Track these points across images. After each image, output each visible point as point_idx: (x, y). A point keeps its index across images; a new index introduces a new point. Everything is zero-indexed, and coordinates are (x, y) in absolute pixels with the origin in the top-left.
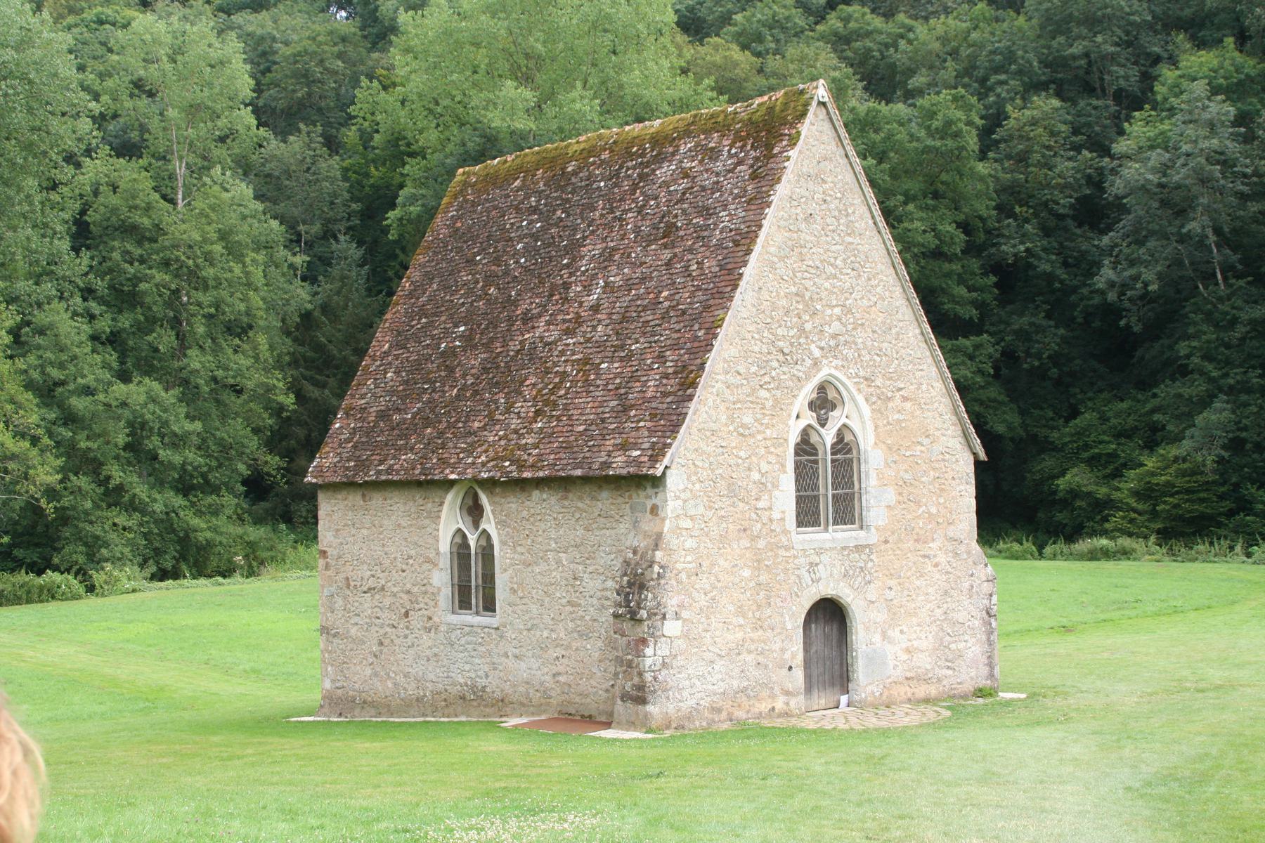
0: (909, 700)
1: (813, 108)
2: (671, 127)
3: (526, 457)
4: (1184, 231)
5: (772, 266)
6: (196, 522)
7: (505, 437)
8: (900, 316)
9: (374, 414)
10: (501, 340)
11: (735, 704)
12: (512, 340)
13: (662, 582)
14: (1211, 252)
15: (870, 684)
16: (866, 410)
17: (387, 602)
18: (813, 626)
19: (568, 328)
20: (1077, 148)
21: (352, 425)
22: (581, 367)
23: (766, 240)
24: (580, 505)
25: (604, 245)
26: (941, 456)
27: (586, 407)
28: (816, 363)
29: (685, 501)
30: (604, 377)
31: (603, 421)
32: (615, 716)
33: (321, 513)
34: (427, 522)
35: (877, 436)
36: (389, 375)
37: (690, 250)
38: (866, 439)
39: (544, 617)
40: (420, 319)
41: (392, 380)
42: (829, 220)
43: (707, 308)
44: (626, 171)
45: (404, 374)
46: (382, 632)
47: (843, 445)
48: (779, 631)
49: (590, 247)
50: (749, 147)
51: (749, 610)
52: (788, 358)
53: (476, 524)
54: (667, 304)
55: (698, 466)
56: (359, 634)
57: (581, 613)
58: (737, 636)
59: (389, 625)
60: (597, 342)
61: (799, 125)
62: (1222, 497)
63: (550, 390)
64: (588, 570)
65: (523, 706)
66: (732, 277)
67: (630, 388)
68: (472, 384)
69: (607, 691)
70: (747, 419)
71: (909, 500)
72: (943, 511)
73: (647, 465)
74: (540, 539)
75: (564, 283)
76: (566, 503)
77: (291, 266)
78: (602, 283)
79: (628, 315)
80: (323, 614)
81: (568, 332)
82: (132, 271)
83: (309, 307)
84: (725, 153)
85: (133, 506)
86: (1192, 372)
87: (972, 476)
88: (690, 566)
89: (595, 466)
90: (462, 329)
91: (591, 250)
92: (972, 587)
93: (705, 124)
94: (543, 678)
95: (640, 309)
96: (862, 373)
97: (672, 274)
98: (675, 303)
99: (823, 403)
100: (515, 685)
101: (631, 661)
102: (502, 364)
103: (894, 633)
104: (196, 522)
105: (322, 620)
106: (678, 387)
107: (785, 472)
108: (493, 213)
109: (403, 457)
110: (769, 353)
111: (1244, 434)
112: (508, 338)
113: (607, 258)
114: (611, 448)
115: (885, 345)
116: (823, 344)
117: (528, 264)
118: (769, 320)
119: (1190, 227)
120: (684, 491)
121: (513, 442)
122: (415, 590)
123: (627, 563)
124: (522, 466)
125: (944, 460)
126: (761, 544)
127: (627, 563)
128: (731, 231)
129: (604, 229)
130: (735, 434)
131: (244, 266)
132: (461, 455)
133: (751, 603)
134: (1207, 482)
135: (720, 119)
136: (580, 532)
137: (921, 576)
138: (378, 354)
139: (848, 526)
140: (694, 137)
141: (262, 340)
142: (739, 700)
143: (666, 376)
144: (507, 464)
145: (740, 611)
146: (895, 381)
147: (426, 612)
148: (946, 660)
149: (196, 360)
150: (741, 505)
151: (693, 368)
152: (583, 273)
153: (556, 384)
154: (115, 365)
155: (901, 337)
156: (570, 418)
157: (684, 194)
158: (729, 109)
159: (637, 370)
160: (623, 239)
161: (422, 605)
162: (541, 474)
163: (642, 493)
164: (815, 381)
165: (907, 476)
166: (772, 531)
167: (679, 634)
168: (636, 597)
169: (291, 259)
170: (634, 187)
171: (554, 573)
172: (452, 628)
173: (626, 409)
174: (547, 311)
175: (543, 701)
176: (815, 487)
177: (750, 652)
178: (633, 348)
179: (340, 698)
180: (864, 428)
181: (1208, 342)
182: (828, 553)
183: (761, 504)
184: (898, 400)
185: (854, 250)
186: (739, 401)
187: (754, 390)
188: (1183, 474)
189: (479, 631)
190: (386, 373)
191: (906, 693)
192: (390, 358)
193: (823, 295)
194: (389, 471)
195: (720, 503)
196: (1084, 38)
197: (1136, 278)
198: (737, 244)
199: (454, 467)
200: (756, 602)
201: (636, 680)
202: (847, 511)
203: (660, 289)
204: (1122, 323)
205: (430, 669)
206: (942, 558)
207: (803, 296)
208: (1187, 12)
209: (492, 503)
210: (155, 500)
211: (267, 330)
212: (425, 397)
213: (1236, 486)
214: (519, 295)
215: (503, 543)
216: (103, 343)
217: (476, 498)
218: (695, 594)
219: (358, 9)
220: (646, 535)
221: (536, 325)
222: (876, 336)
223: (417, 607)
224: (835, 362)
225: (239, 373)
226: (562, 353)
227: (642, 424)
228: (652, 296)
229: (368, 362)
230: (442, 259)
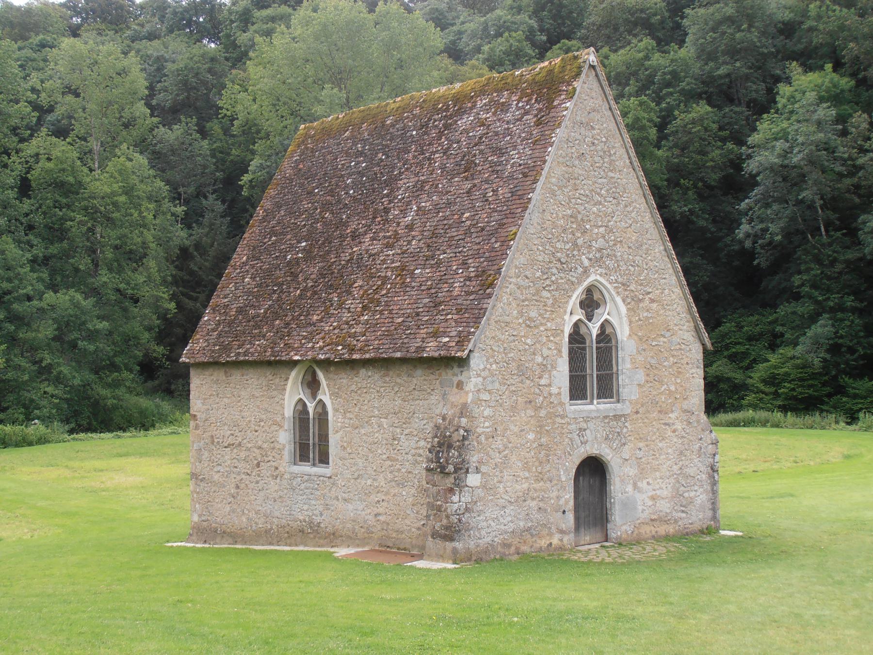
0: (653, 537)
1: (585, 70)
2: (469, 88)
3: (355, 343)
4: (800, 197)
6: (104, 392)
7: (339, 327)
8: (648, 236)
9: (235, 310)
10: (335, 252)
11: (522, 541)
12: (343, 252)
13: (466, 443)
14: (817, 212)
15: (625, 524)
16: (623, 309)
17: (243, 455)
18: (581, 478)
19: (388, 242)
20: (724, 140)
21: (217, 318)
22: (399, 272)
23: (549, 172)
24: (398, 380)
25: (417, 178)
26: (678, 346)
27: (403, 302)
28: (586, 272)
29: (484, 379)
30: (418, 280)
31: (418, 314)
32: (427, 549)
33: (192, 386)
34: (275, 393)
35: (631, 329)
36: (246, 280)
37: (487, 181)
38: (623, 331)
39: (369, 468)
40: (271, 237)
41: (249, 284)
42: (597, 159)
43: (501, 225)
44: (434, 123)
45: (258, 279)
46: (239, 478)
47: (606, 337)
48: (556, 482)
49: (405, 181)
50: (533, 101)
51: (533, 465)
52: (565, 266)
53: (314, 395)
54: (468, 223)
55: (494, 351)
56: (221, 479)
57: (398, 466)
58: (523, 486)
59: (244, 473)
60: (411, 253)
61: (574, 83)
62: (824, 384)
63: (374, 290)
64: (405, 433)
65: (350, 539)
66: (522, 201)
67: (439, 289)
68: (312, 286)
69: (419, 529)
70: (533, 314)
71: (654, 380)
72: (680, 389)
73: (455, 349)
74: (366, 407)
75: (385, 208)
76: (387, 379)
77: (173, 214)
79: (437, 231)
80: (193, 463)
81: (389, 246)
82: (61, 214)
83: (187, 243)
84: (514, 106)
85: (58, 380)
86: (803, 297)
87: (701, 361)
88: (488, 430)
89: (413, 349)
90: (304, 244)
91: (407, 182)
92: (701, 448)
93: (497, 84)
94: (366, 518)
95: (446, 227)
96: (620, 280)
97: (473, 200)
98: (475, 222)
100: (344, 522)
101: (441, 506)
102: (336, 271)
103: (643, 485)
104: (104, 392)
105: (192, 468)
106: (479, 288)
107: (561, 356)
108: (328, 157)
109: (257, 343)
110: (550, 262)
111: (841, 341)
112: (340, 251)
113: (419, 189)
114: (425, 336)
115: (638, 258)
116: (591, 256)
117: (356, 194)
118: (550, 236)
119: (805, 195)
120: (484, 370)
121: (344, 331)
122: (265, 446)
123: (437, 427)
124: (353, 350)
125: (680, 349)
126: (543, 413)
127: (437, 427)
128: (520, 165)
129: (416, 167)
130: (523, 325)
131: (141, 212)
132: (303, 341)
133: (534, 460)
134: (813, 373)
135: (509, 81)
136: (399, 402)
137: (663, 439)
138: (238, 264)
139: (608, 400)
140: (488, 95)
141: (152, 264)
142: (524, 538)
143: (469, 279)
144: (340, 348)
145: (526, 467)
146: (645, 286)
147: (274, 464)
148: (681, 506)
149: (104, 277)
150: (528, 382)
151: (492, 272)
152: (400, 200)
153: (379, 286)
154: (47, 279)
155: (649, 252)
156: (390, 312)
157: (481, 138)
158: (517, 73)
159: (445, 274)
160: (432, 174)
161: (270, 458)
162: (367, 356)
163: (450, 372)
164: (585, 284)
165: (653, 361)
166: (551, 403)
167: (479, 484)
168: (445, 455)
169: (173, 209)
170: (441, 134)
171: (377, 435)
172: (294, 476)
173: (437, 305)
174: (371, 230)
175: (366, 535)
176: (584, 369)
177: (533, 499)
178: (441, 257)
179: (205, 528)
180: (621, 323)
181: (815, 276)
182: (593, 421)
183: (543, 382)
184: (647, 302)
185: (615, 182)
186: (526, 300)
187: (538, 292)
188: (797, 367)
189: (316, 479)
190: (244, 278)
191: (651, 532)
192: (247, 267)
193: (592, 217)
194: (246, 354)
195: (512, 381)
196: (727, 64)
197: (765, 230)
198: (525, 175)
199: (297, 351)
200: (538, 459)
201: (445, 521)
203: (463, 211)
204: (755, 263)
205: (276, 508)
206: (679, 426)
207: (576, 218)
208: (800, 47)
209: (327, 379)
210: (74, 377)
211: (155, 258)
212: (275, 296)
213: (835, 378)
214: (349, 218)
215: (336, 410)
216: (39, 265)
217: (314, 374)
218: (491, 452)
219: (223, 40)
220: (453, 405)
221: (363, 241)
222: (631, 251)
223: (266, 459)
225: (136, 287)
226: (384, 262)
227: (449, 317)
228: (456, 217)
229: (230, 271)
230: (288, 192)
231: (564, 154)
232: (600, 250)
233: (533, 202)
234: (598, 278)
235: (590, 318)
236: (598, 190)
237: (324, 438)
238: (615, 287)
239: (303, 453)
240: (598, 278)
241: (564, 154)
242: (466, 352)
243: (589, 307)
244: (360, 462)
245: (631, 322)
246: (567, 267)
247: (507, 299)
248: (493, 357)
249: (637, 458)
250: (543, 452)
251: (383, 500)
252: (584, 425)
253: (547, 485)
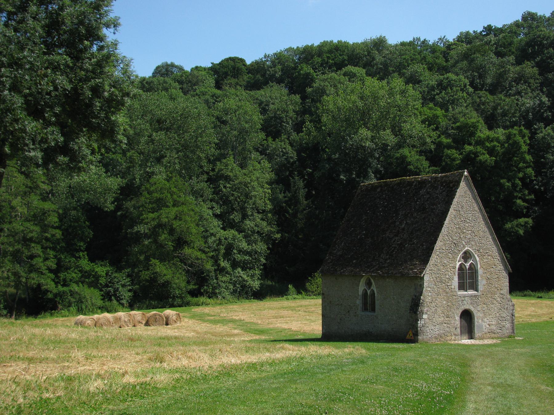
28: (464, 247)
42: (468, 207)
78: (405, 222)
96: (477, 249)
99: (467, 256)
123: (413, 299)
165: (489, 277)
201: (415, 330)
215: (377, 292)
224: (469, 246)
226: (394, 241)
234: (468, 248)
239: (365, 309)
240: (468, 248)
245: (480, 263)
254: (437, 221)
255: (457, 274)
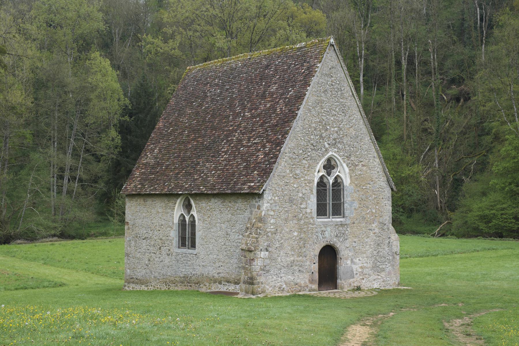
5: (310, 111)
8: (362, 132)
16: (347, 170)
17: (153, 243)
24: (230, 205)
28: (327, 150)
29: (271, 204)
36: (156, 151)
38: (347, 181)
46: (150, 255)
47: (338, 184)
51: (296, 249)
53: (189, 212)
58: (291, 259)
59: (153, 253)
70: (298, 172)
88: (273, 230)
96: (346, 154)
99: (329, 166)
107: (313, 194)
110: (307, 145)
120: (271, 200)
122: (164, 238)
125: (379, 191)
130: (292, 177)
133: (297, 246)
136: (230, 216)
144: (201, 188)
145: (293, 249)
148: (378, 272)
150: (294, 206)
161: (166, 245)
163: (254, 201)
164: (326, 157)
166: (307, 217)
171: (219, 232)
177: (296, 266)
180: (346, 177)
183: (302, 206)
193: (330, 122)
201: (249, 275)
202: (338, 210)
209: (195, 203)
215: (199, 220)
231: (316, 90)
232: (335, 139)
233: (299, 115)
234: (334, 154)
235: (329, 174)
236: (335, 108)
237: (193, 234)
238: (343, 159)
239: (183, 243)
240: (334, 154)
241: (316, 90)
242: (262, 190)
243: (328, 169)
244: (211, 247)
245: (351, 177)
246: (317, 148)
247: (284, 164)
248: (276, 194)
249: (353, 247)
250: (302, 242)
251: (222, 266)
252: (324, 229)
253: (304, 259)
254: (287, 111)
255: (315, 191)
